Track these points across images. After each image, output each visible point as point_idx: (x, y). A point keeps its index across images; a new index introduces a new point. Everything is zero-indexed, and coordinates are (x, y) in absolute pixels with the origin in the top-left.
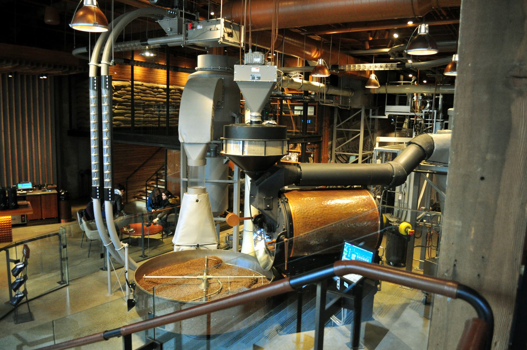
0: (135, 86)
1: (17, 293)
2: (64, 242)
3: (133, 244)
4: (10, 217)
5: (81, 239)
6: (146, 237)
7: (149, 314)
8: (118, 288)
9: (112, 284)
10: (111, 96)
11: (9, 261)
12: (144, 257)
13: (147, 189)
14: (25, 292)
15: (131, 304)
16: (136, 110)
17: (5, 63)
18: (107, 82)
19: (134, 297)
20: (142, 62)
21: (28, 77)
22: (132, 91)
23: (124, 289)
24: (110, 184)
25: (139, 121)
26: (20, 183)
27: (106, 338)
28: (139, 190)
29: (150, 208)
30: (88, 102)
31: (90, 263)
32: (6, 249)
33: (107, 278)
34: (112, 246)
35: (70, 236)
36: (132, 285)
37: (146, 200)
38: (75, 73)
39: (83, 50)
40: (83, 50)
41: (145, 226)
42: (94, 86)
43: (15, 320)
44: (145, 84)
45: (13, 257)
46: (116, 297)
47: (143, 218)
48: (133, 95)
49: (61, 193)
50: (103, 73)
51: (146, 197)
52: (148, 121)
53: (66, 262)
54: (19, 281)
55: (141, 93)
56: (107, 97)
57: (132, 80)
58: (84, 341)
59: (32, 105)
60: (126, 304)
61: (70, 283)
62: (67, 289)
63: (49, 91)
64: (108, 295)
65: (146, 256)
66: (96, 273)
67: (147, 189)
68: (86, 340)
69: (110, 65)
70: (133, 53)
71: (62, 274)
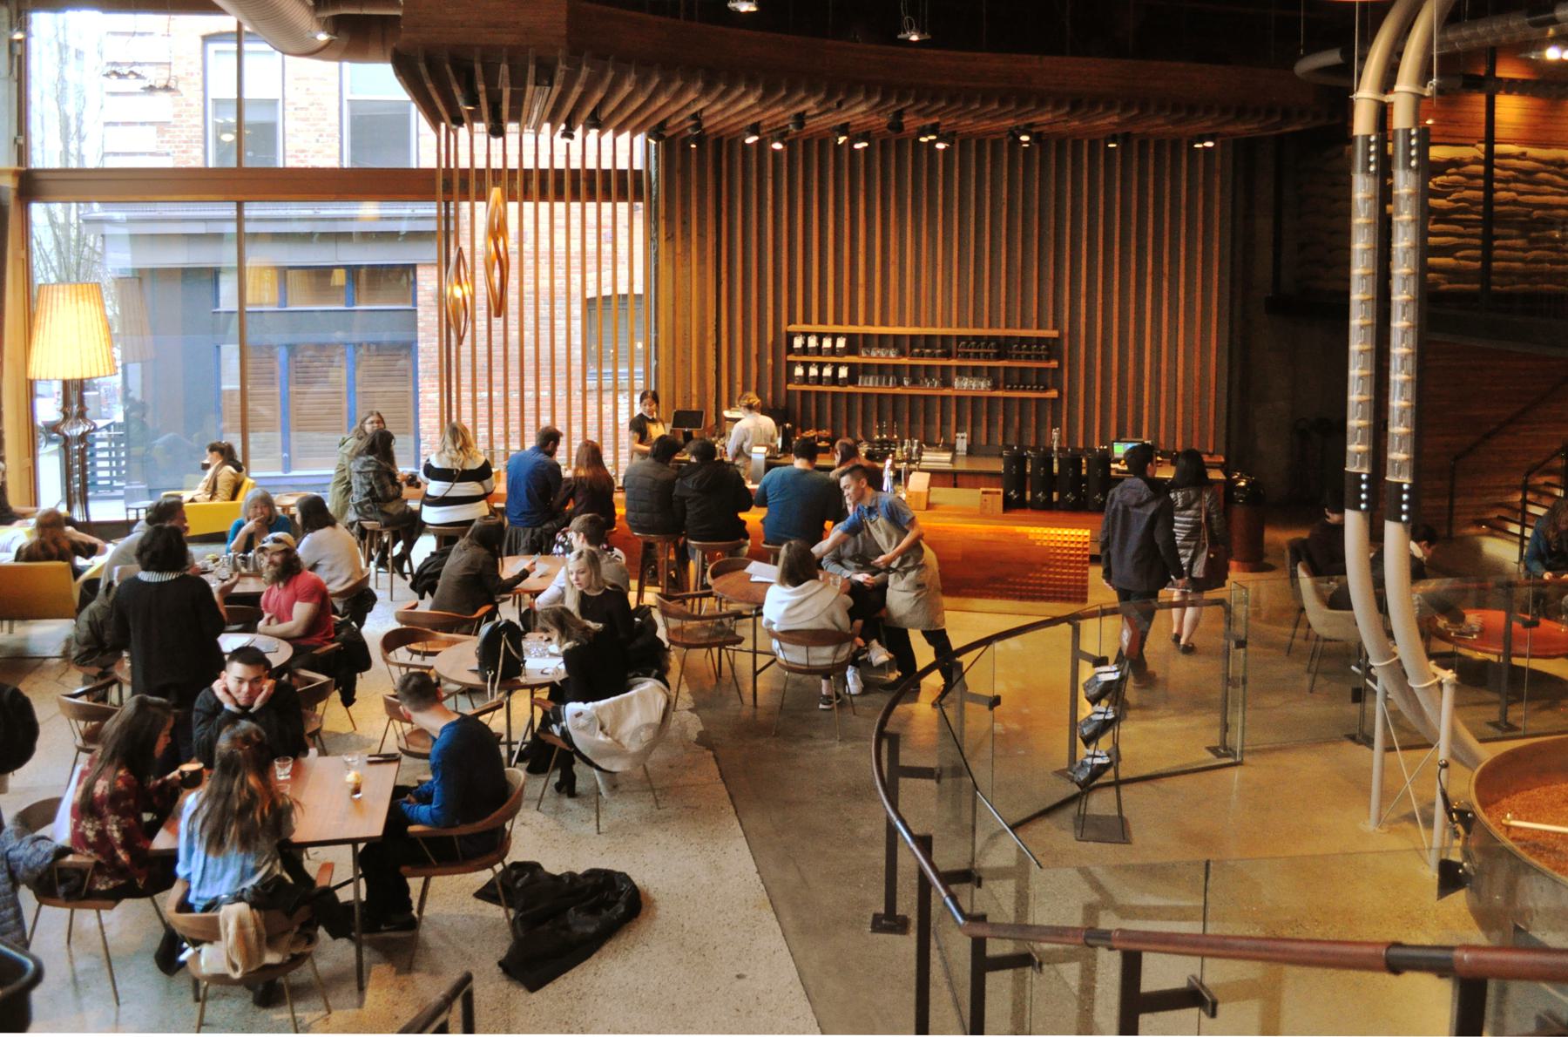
0: (1496, 161)
1: (1091, 752)
2: (1239, 630)
3: (1472, 676)
4: (1087, 533)
5: (1290, 630)
6: (1516, 661)
7: (1517, 929)
8: (1406, 811)
9: (1386, 796)
10: (1424, 194)
11: (1077, 655)
12: (1506, 729)
13: (1525, 502)
14: (1115, 755)
15: (1450, 877)
16: (1497, 238)
17: (1101, 109)
18: (1411, 148)
19: (1467, 855)
20: (1524, 81)
21: (1159, 145)
22: (1489, 177)
23: (1429, 822)
24: (1407, 469)
25: (1506, 273)
26: (1118, 441)
27: (1395, 966)
28: (1498, 499)
29: (1536, 566)
30: (1347, 214)
31: (1311, 709)
32: (1073, 619)
33: (1370, 770)
34: (1399, 673)
35: (1257, 614)
36: (1462, 814)
37: (1522, 537)
38: (1298, 128)
39: (1333, 57)
40: (1333, 57)
41: (1517, 625)
42: (1411, 158)
43: (1076, 827)
44: (1533, 152)
45: (1090, 645)
46: (1395, 842)
47: (1509, 595)
48: (1489, 190)
49: (1237, 481)
50: (1401, 119)
51: (1523, 525)
52: (1541, 274)
53: (1240, 691)
54: (1101, 717)
55: (1516, 180)
56: (1410, 195)
57: (1490, 140)
58: (1314, 953)
59: (1167, 226)
60: (1432, 875)
61: (1247, 759)
62: (1236, 773)
63: (1217, 180)
64: (1370, 826)
65: (1511, 728)
66: (1331, 747)
67: (1525, 502)
68: (1322, 953)
69: (1422, 97)
70: (1492, 55)
71: (1226, 728)
